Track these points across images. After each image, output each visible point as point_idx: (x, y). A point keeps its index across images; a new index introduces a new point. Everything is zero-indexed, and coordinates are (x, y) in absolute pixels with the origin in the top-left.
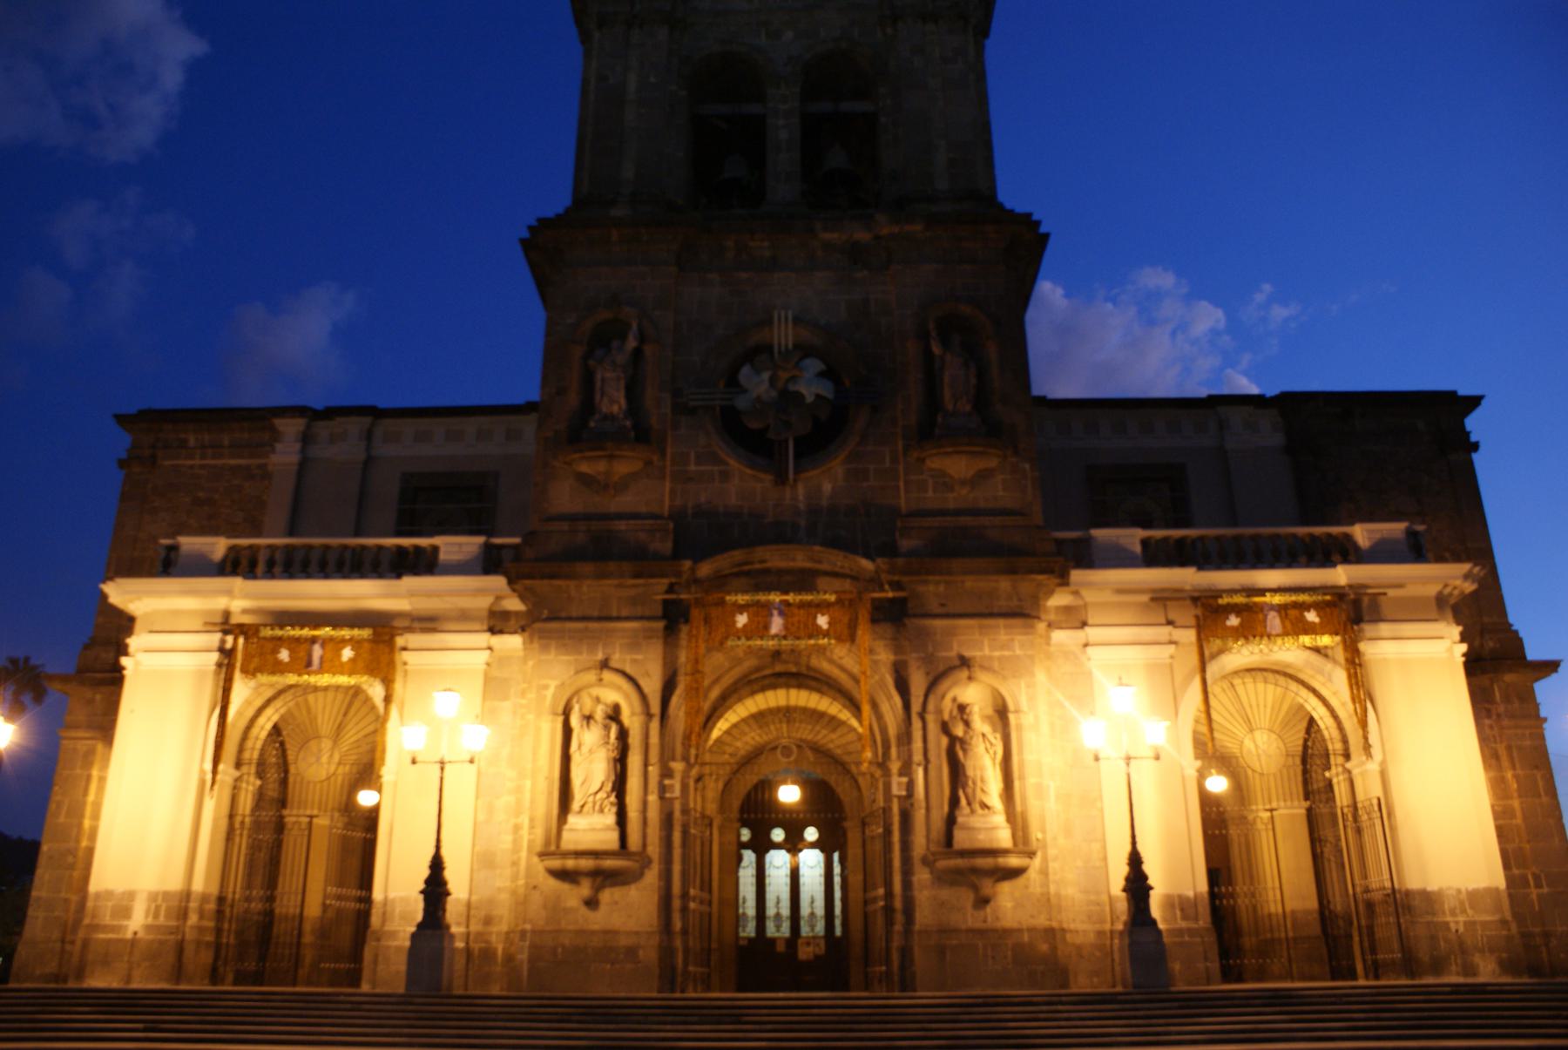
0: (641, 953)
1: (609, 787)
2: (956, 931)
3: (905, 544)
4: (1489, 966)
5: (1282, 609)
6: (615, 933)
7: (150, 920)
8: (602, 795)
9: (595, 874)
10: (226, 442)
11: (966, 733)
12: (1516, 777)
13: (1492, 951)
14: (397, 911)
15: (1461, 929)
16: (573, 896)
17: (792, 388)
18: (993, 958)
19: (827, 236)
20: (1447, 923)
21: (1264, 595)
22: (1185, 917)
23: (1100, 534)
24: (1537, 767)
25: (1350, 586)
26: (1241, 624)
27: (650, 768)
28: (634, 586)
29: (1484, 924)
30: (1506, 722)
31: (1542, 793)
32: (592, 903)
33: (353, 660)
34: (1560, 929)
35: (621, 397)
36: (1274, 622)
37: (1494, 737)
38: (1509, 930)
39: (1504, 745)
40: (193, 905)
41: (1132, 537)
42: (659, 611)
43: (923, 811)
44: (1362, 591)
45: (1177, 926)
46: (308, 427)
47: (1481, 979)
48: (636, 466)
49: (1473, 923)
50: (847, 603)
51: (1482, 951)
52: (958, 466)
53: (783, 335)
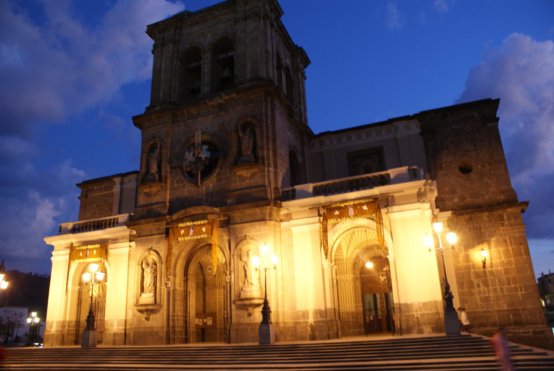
0: (159, 333)
1: (152, 285)
2: (242, 324)
3: (229, 201)
4: (428, 330)
5: (354, 206)
6: (154, 327)
7: (57, 329)
8: (150, 288)
9: (147, 310)
10: (103, 187)
11: (247, 260)
12: (512, 249)
13: (429, 324)
14: (109, 323)
15: (419, 317)
16: (143, 316)
17: (199, 156)
18: (252, 332)
19: (211, 103)
20: (414, 315)
21: (348, 202)
22: (321, 317)
23: (297, 187)
24: (521, 244)
25: (380, 194)
26: (340, 214)
27: (162, 279)
28: (157, 225)
29: (428, 314)
30: (508, 228)
31: (523, 254)
32: (147, 319)
33: (96, 254)
34: (529, 307)
35: (156, 169)
36: (351, 211)
37: (505, 234)
38: (439, 316)
39: (508, 237)
40: (67, 324)
41: (310, 187)
42: (164, 231)
43: (233, 287)
44: (388, 195)
45: (318, 320)
46: (122, 179)
47: (425, 335)
48: (159, 188)
49: (424, 314)
50: (210, 223)
51: (426, 324)
52: (245, 173)
53: (198, 139)
